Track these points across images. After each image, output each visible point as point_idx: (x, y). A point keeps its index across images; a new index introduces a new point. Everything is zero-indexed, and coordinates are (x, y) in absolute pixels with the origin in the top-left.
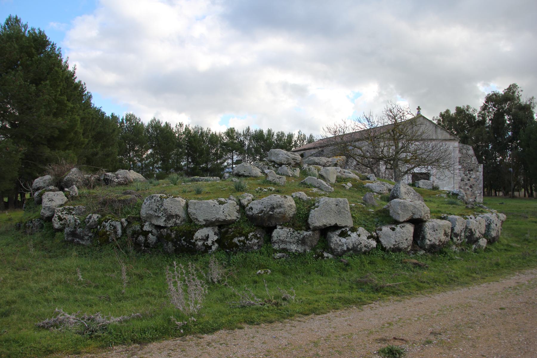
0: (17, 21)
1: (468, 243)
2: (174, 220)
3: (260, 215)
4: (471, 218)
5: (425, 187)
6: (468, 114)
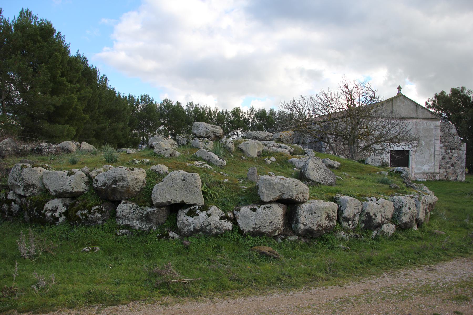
0: (29, 13)
1: (365, 228)
2: (32, 189)
3: (103, 188)
4: (372, 200)
5: (374, 164)
6: (463, 95)
